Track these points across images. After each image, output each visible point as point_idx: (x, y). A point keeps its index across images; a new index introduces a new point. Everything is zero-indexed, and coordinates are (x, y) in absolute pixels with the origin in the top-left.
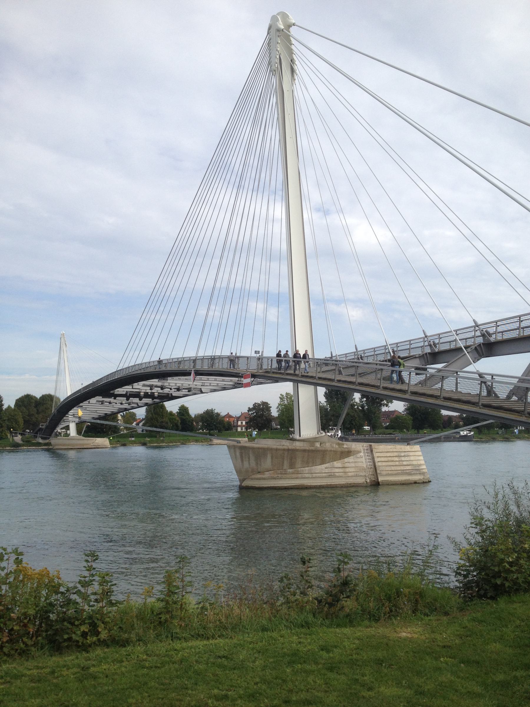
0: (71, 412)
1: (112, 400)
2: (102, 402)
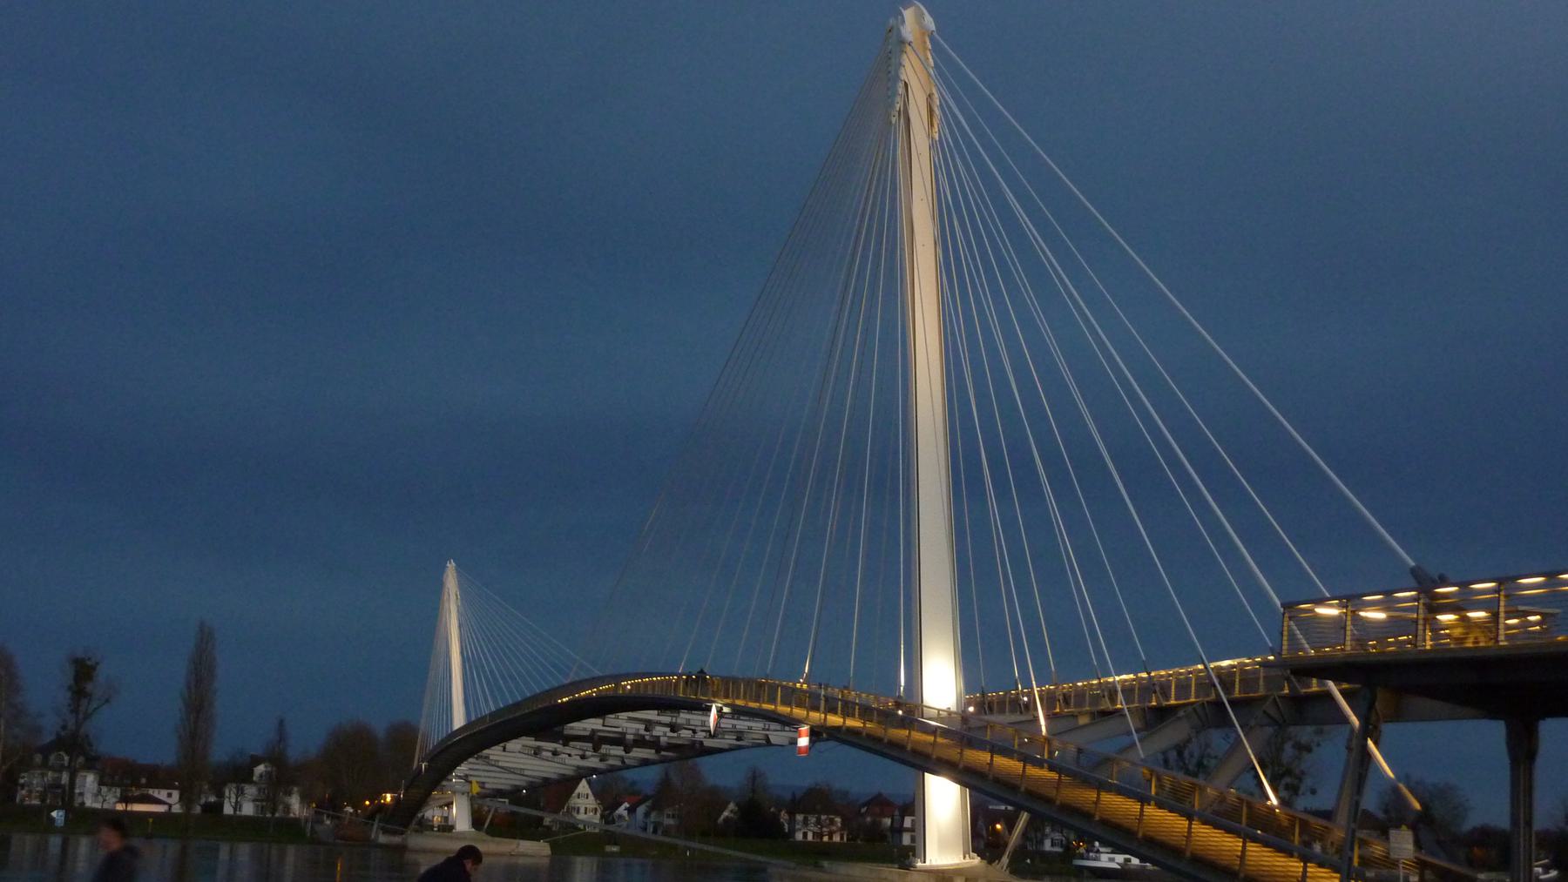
0: (463, 769)
1: (558, 747)
2: (537, 752)
